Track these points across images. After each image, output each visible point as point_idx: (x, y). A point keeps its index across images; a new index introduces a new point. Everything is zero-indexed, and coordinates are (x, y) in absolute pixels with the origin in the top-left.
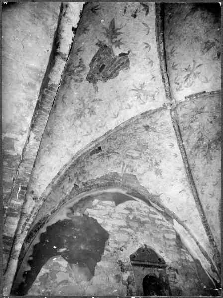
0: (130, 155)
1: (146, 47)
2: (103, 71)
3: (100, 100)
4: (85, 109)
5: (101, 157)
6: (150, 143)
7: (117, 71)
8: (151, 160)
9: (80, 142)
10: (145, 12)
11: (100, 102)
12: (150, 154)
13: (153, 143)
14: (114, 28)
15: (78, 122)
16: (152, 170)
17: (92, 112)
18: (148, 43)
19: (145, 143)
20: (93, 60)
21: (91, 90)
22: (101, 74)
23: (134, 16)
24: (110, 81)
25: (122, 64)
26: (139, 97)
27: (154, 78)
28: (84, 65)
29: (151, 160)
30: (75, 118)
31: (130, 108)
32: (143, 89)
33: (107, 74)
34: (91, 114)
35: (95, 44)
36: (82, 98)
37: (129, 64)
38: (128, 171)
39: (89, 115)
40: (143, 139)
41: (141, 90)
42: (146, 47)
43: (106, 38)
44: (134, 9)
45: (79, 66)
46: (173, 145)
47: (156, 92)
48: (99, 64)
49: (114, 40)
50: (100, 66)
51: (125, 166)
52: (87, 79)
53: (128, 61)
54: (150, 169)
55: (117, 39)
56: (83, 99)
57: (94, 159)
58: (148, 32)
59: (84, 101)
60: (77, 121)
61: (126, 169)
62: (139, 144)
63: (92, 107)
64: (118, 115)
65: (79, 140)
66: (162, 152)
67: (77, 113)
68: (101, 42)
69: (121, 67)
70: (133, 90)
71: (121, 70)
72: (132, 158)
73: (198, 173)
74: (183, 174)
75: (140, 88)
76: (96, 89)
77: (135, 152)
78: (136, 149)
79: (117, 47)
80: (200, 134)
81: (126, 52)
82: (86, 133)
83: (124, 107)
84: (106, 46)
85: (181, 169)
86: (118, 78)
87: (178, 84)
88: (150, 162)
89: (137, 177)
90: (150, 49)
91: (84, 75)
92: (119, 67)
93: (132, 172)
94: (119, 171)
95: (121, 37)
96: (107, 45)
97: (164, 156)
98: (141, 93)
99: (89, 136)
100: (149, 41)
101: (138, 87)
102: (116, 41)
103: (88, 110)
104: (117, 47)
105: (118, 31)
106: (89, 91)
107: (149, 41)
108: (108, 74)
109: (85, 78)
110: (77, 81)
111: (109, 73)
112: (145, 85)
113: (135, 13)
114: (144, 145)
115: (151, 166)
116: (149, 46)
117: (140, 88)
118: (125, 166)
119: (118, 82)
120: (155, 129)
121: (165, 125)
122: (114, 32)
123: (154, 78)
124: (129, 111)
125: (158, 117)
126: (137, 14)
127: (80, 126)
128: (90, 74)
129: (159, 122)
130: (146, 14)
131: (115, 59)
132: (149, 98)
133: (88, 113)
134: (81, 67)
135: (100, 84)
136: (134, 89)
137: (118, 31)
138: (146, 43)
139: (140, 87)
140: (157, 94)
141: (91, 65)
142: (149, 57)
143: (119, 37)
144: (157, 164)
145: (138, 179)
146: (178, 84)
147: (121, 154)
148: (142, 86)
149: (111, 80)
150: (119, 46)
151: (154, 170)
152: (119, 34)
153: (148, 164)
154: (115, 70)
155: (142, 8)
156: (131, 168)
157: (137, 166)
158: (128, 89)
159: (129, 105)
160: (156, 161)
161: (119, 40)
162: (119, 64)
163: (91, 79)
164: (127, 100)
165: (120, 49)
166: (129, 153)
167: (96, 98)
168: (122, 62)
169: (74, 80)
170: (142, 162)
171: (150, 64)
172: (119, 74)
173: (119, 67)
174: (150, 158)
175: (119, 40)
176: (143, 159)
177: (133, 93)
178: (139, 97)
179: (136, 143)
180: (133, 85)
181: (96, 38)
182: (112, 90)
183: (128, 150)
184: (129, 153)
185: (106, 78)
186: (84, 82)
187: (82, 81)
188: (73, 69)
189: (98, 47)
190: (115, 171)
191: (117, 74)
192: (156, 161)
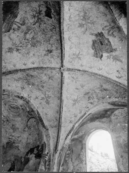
0: (29, 32)
1: (100, 68)
2: (100, 43)
3: (84, 34)
4: (86, 22)
5: (38, 11)
6: (36, 49)
7: (95, 50)
8: (21, 46)
9: (69, 10)
10: (117, 76)
11: (83, 33)
12: (26, 46)
13: (35, 51)
14: (118, 60)
15: (82, 14)
16: (13, 46)
17: (81, 25)
18: (102, 70)
19: (37, 46)
20: (109, 42)
21: (94, 31)
22: (98, 41)
23: (118, 71)
24: (91, 43)
25: (97, 54)
26: (74, 55)
27: (82, 66)
28: (111, 36)
29: (21, 46)
30: (86, 13)
31: (70, 48)
32: (77, 58)
33: (96, 44)
34: (80, 24)
35: (117, 48)
36: (94, 24)
37: (95, 57)
38: (15, 26)
39: (81, 23)
40: (41, 45)
41: (78, 57)
42: (100, 68)
43: (116, 54)
44: (121, 73)
45: (112, 33)
46: (33, 64)
47: (73, 64)
48: (105, 43)
49: (112, 57)
50: (103, 43)
51: (20, 26)
52: (102, 33)
53: (97, 57)
54: (14, 44)
55: (111, 58)
56: (92, 24)
57: (39, 6)
58: (107, 73)
59: (91, 24)
60: (83, 14)
61: (17, 25)
62: (37, 41)
63: (84, 27)
64: (69, 40)
65: (71, 10)
66: (28, 55)
67: (88, 16)
68: (115, 51)
69: (96, 52)
70: (79, 53)
71: (93, 51)
72: (26, 33)
73: (90, 115)
74: (11, 68)
75: (78, 57)
76: (92, 34)
77: (31, 36)
78: (33, 38)
79: (107, 56)
80: (36, 76)
81: (102, 59)
82: (72, 16)
83: (73, 45)
84: (111, 51)
85: (15, 67)
86: (91, 49)
87: (72, 74)
88: (20, 45)
89: (8, 33)
90: (98, 70)
91: (105, 33)
92: (96, 51)
93: (14, 29)
94: (17, 20)
95: (111, 60)
96: (111, 53)
97: (24, 56)
98: (75, 56)
99: (68, 18)
100: (102, 71)
101: (80, 56)
102: (111, 57)
103: (83, 24)
104: (107, 56)
105: (115, 61)
106: (94, 30)
107: (102, 71)
108: (96, 45)
109: (103, 32)
110: (106, 27)
111: (96, 45)
112: (80, 60)
113: (119, 72)
114: (35, 45)
115: (16, 45)
116: (100, 70)
117: (78, 57)
118: (20, 26)
119: (88, 47)
120: (47, 55)
121: (49, 62)
122: (116, 59)
123: (82, 66)
124: (69, 47)
125: (56, 60)
126: (118, 73)
127: (79, 14)
128: (103, 35)
129: (52, 59)
130: (116, 76)
131: (102, 52)
132: (71, 60)
133: (82, 23)
134: (111, 34)
135: (94, 38)
136: (80, 54)
137: (115, 61)
138: (102, 69)
139: (79, 57)
140: (72, 64)
141: (108, 39)
142: (94, 67)
143: (112, 60)
144: (18, 50)
145: (6, 33)
146: (72, 74)
147: (33, 26)
148: (80, 58)
149: (92, 44)
150: (107, 57)
151: (13, 47)
152: (113, 61)
153: (18, 44)
154: (96, 49)
155: (120, 76)
156: (17, 30)
157: (17, 34)
158: (81, 51)
159: (72, 48)
160: (21, 50)
161: (110, 59)
162: (97, 52)
163: (100, 35)
164: (75, 48)
165: (106, 57)
166: (31, 32)
167: (87, 31)
168: (98, 54)
169: (108, 26)
170: (21, 39)
171: (90, 67)
172: (92, 50)
173: (96, 51)
174: (23, 46)
175: (110, 59)
176: (23, 40)
177: (78, 52)
178: (74, 54)
179: (39, 40)
180: (82, 54)
181: (120, 51)
182: (86, 42)
183: (34, 33)
184: (31, 32)
185: (94, 42)
186: (102, 30)
187: (103, 29)
188: (114, 30)
189: (114, 48)
190: (18, 17)
191: (93, 49)
192: (21, 50)
